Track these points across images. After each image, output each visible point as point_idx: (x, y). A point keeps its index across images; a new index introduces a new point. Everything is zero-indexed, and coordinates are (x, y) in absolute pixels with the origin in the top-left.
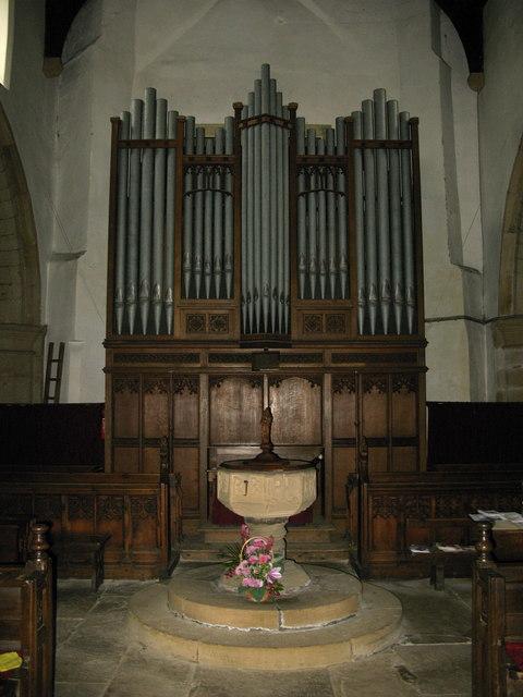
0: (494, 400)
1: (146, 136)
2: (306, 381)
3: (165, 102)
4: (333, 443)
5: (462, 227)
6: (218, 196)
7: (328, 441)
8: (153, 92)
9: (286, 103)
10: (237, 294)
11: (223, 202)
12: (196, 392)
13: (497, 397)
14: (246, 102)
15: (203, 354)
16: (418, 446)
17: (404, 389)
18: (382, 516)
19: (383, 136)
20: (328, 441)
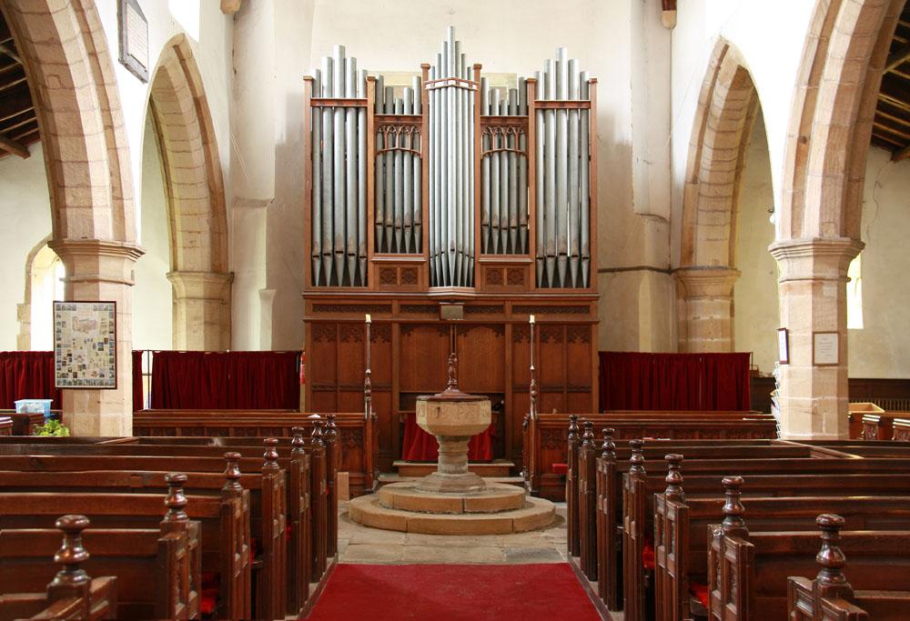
0: (676, 351)
1: (337, 96)
2: (491, 331)
3: (354, 61)
4: (391, 387)
5: (28, 513)
6: (352, 249)
7: (509, 386)
8: (342, 50)
9: (470, 63)
10: (425, 249)
11: (463, 93)
12: (388, 341)
13: (679, 348)
14: (434, 63)
15: (395, 305)
16: (391, 392)
17: (578, 340)
18: (549, 448)
19: (565, 98)
20: (509, 386)
